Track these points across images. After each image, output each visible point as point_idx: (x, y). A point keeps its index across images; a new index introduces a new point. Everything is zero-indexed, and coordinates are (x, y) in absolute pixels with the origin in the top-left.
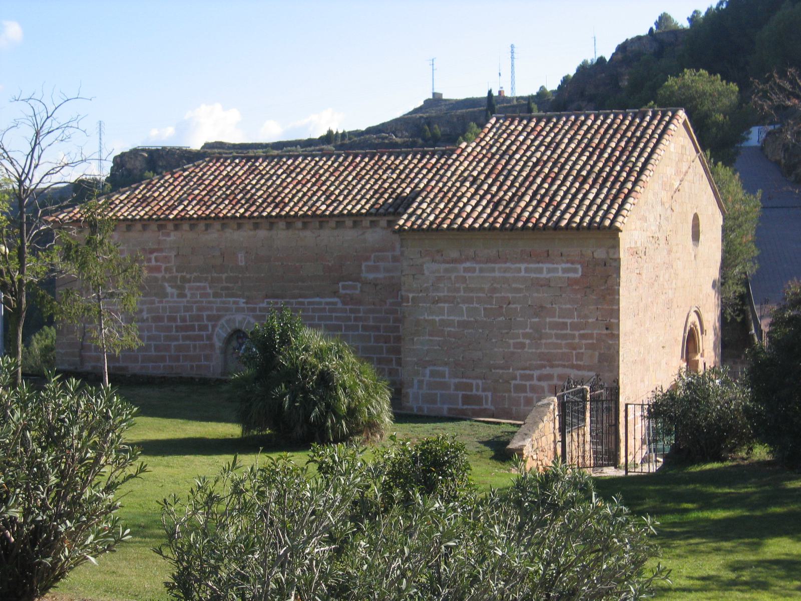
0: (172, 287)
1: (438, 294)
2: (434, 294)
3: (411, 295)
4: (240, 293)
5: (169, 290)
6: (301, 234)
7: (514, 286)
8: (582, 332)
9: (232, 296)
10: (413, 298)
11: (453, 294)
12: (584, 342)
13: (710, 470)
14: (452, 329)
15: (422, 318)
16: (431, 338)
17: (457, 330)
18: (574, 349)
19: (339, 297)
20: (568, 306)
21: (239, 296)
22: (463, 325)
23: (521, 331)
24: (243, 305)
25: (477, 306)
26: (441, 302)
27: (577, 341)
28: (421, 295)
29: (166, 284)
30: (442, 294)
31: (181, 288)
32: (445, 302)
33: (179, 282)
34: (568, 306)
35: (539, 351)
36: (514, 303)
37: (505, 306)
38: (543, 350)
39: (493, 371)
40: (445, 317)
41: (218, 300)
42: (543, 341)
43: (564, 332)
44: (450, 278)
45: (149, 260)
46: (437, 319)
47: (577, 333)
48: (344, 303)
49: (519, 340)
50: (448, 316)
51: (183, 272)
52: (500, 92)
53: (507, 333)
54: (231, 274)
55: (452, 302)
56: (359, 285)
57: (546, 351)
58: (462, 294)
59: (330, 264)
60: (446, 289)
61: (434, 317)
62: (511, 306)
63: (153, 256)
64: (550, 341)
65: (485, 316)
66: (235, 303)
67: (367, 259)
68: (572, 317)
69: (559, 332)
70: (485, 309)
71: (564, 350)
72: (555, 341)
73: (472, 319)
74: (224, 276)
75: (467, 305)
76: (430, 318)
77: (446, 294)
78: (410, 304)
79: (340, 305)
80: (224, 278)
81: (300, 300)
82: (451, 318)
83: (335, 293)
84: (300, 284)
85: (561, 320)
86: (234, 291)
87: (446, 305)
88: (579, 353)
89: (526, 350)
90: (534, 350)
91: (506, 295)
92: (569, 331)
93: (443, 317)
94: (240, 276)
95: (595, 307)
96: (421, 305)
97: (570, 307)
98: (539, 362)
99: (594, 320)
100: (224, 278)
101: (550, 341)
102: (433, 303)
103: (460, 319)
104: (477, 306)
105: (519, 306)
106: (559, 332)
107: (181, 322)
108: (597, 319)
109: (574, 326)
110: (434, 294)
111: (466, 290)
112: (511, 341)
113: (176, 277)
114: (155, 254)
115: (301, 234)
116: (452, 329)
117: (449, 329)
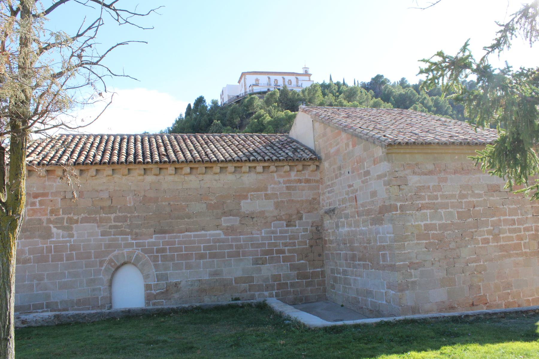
0: (58, 228)
1: (421, 202)
2: (418, 202)
3: (399, 204)
4: (128, 230)
5: (54, 230)
6: (186, 178)
7: (476, 192)
8: (525, 226)
9: (122, 233)
10: (401, 206)
11: (433, 201)
12: (527, 233)
13: (350, 319)
14: (435, 232)
15: (410, 224)
16: (418, 242)
17: (439, 232)
18: (522, 240)
19: (221, 230)
20: (514, 206)
21: (127, 234)
22: (443, 227)
23: (485, 229)
24: (130, 241)
25: (452, 210)
26: (424, 209)
27: (522, 233)
28: (407, 203)
29: (51, 226)
30: (424, 202)
31: (69, 229)
32: (428, 208)
33: (65, 224)
34: (514, 206)
35: (499, 244)
36: (478, 206)
37: (471, 209)
38: (502, 243)
39: (469, 265)
40: (429, 222)
41: (107, 237)
42: (501, 236)
43: (514, 227)
44: (429, 187)
45: (33, 204)
46: (422, 224)
47: (522, 227)
48: (225, 234)
49: (484, 237)
50: (431, 220)
51: (70, 214)
52: (523, 5)
53: (476, 231)
54: (120, 214)
55: (433, 208)
56: (238, 219)
57: (504, 243)
58: (439, 200)
59: (213, 202)
60: (426, 197)
61: (420, 223)
62: (476, 208)
63: (37, 200)
64: (505, 235)
65: (459, 219)
66: (123, 239)
67: (246, 197)
68: (516, 214)
69: (511, 227)
70: (458, 212)
71: (515, 242)
72: (509, 235)
73: (449, 222)
74: (113, 216)
75: (444, 210)
76: (417, 223)
77: (427, 201)
78: (399, 212)
79: (223, 236)
80: (112, 218)
81: (187, 233)
82: (434, 222)
83: (218, 227)
84: (186, 220)
85: (510, 218)
86: (123, 229)
87: (428, 211)
88: (525, 243)
89: (491, 244)
90: (496, 244)
91: (471, 200)
92: (516, 226)
93: (427, 222)
94: (129, 215)
95: (530, 206)
96: (408, 212)
97: (516, 207)
98: (500, 253)
99: (531, 216)
100: (112, 218)
101: (505, 235)
102: (417, 210)
103: (440, 222)
104: (452, 210)
105: (481, 208)
106: (511, 227)
107: (243, 242)
108: (533, 215)
109: (520, 222)
110: (418, 202)
111: (443, 197)
112: (480, 238)
113: (63, 218)
114: (39, 199)
115: (186, 178)
116: (435, 232)
117: (432, 232)
